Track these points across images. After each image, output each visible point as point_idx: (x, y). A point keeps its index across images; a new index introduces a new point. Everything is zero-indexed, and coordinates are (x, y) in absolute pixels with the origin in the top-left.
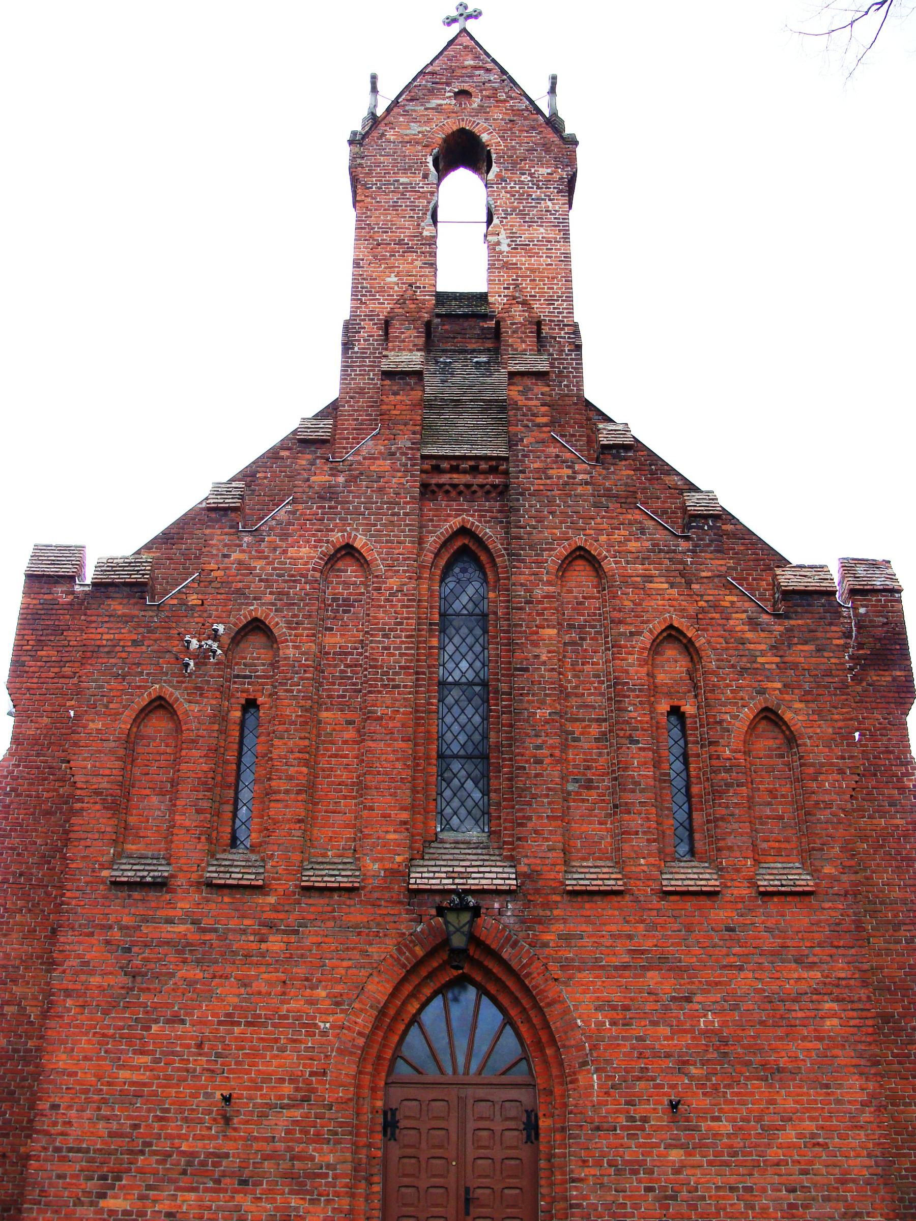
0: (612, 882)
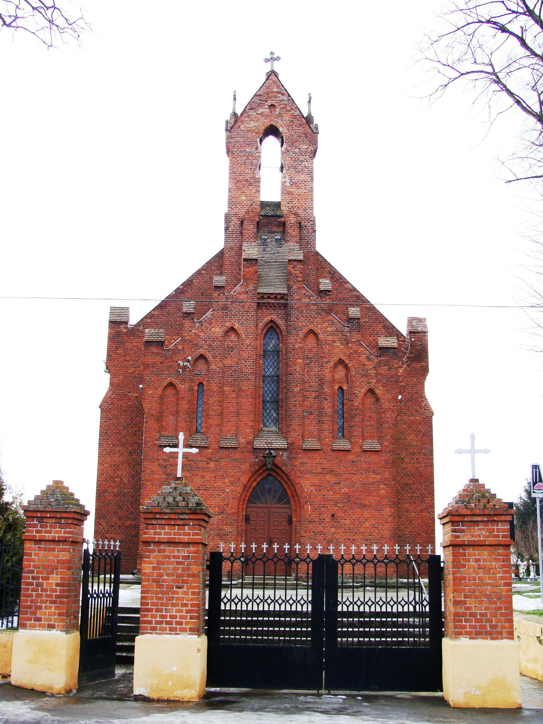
0: (317, 446)
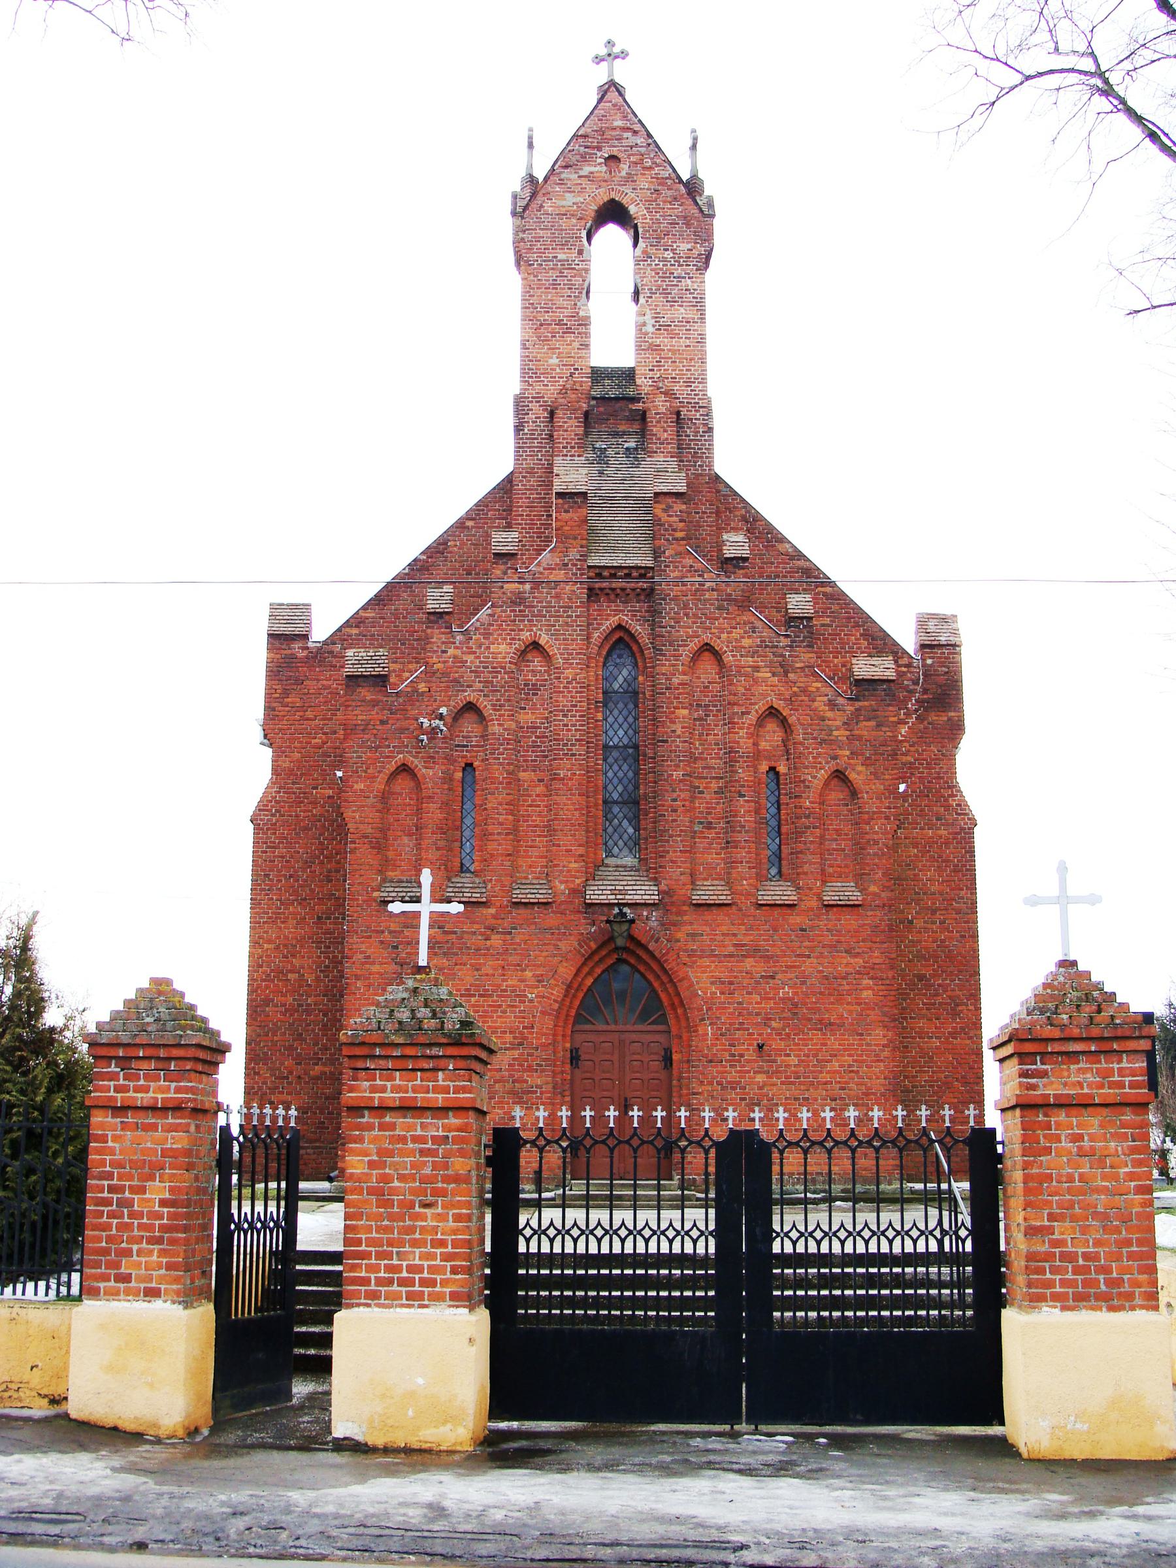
0: (724, 897)
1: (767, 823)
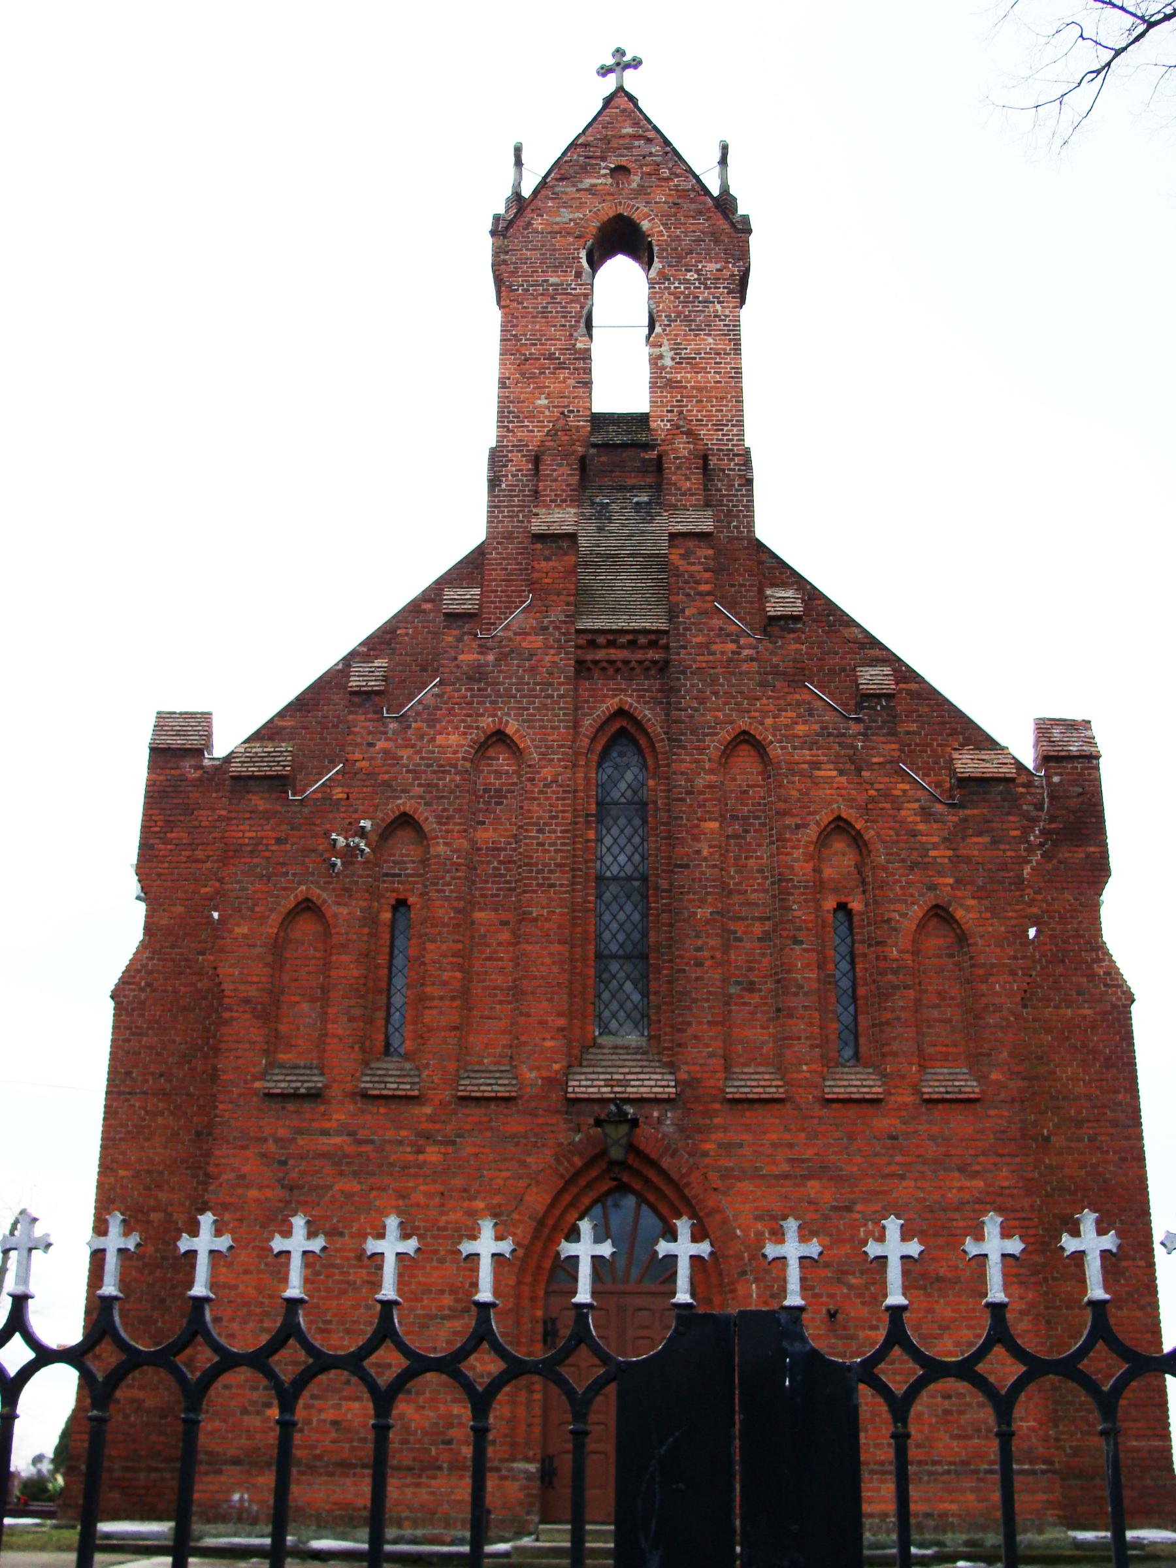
0: (773, 1090)
1: (836, 982)
